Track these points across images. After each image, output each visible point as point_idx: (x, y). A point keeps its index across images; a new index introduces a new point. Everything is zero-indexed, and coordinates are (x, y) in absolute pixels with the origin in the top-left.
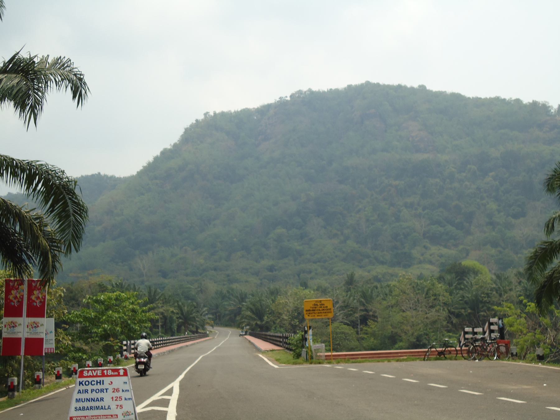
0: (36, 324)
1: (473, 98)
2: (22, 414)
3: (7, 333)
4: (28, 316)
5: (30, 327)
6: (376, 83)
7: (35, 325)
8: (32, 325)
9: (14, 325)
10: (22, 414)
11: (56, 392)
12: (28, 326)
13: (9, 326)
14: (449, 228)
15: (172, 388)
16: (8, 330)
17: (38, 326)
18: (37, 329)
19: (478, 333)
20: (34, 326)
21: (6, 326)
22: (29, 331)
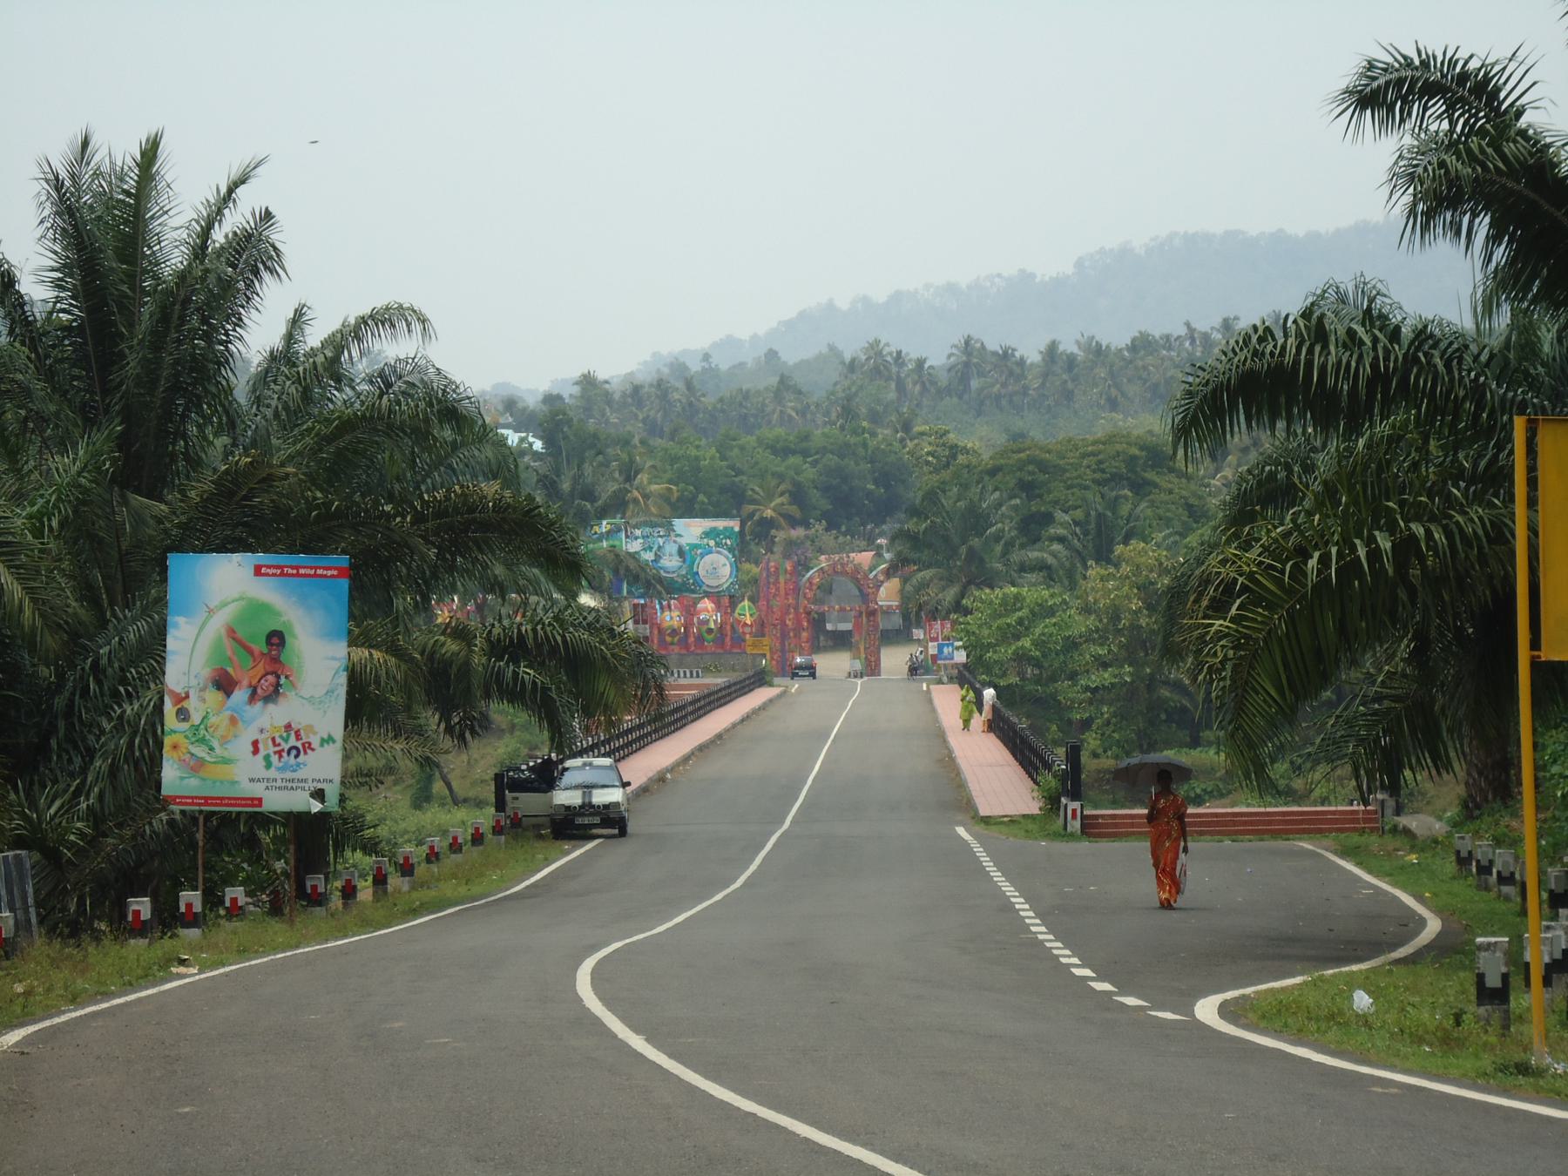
0: (298, 737)
1: (721, 340)
2: (1356, 582)
3: (264, 784)
4: (1540, 650)
5: (267, 748)
6: (843, 304)
7: (293, 742)
8: (278, 740)
9: (299, 745)
10: (1356, 582)
11: (253, 962)
12: (255, 744)
13: (272, 749)
14: (1386, 703)
15: (981, 714)
16: (268, 765)
17: (308, 747)
18: (302, 757)
19: (540, 745)
20: (286, 747)
21: (261, 746)
22: (263, 773)
